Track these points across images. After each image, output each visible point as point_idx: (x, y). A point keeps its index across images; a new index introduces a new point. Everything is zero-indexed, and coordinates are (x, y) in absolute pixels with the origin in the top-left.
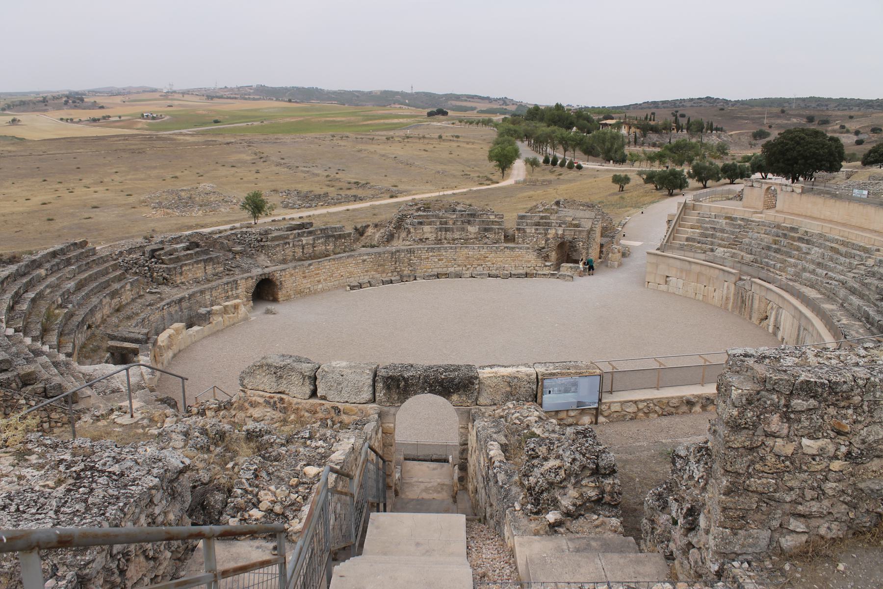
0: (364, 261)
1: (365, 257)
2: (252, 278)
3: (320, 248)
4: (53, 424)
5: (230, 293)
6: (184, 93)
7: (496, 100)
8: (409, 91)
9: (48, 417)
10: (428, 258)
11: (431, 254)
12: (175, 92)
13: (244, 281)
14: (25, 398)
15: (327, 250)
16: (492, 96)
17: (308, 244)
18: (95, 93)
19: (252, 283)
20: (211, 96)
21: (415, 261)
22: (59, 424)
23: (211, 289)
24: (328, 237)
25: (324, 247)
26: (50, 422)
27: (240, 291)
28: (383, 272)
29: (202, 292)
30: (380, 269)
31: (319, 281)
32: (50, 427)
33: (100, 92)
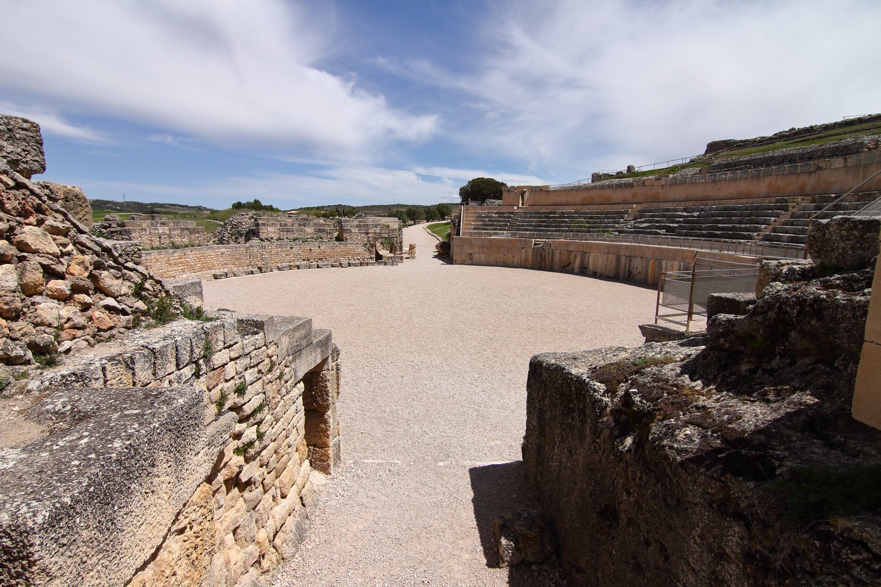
0: (223, 254)
17: (164, 234)
28: (240, 266)
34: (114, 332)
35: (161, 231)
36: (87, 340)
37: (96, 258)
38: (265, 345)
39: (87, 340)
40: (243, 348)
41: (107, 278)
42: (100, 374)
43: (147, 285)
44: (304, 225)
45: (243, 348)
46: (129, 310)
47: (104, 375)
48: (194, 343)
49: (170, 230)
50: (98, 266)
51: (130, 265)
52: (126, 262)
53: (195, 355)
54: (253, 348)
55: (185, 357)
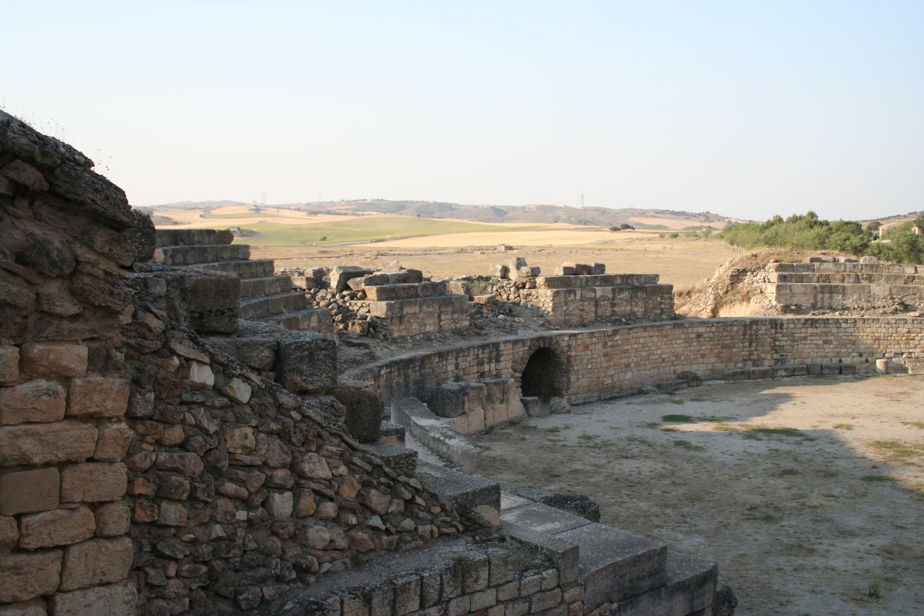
0: (699, 335)
1: (702, 330)
2: (523, 342)
3: (623, 308)
4: (307, 501)
5: (486, 367)
6: (279, 208)
7: (695, 216)
8: (578, 205)
9: (292, 467)
10: (805, 338)
11: (810, 330)
12: (267, 207)
13: (510, 346)
14: (214, 363)
15: (633, 313)
16: (689, 211)
17: (604, 298)
18: (165, 207)
19: (523, 351)
20: (313, 211)
21: (784, 342)
22: (329, 508)
23: (459, 352)
24: (635, 289)
25: (628, 308)
26: (297, 490)
27: (502, 364)
28: (730, 359)
29: (442, 355)
30: (725, 353)
31: (628, 366)
32: (296, 513)
33: (173, 208)
34: (372, 555)
35: (599, 293)
36: (344, 563)
37: (365, 477)
38: (559, 586)
39: (344, 563)
40: (519, 589)
41: (376, 498)
42: (338, 606)
43: (419, 500)
44: (870, 279)
45: (519, 589)
46: (393, 530)
47: (342, 606)
48: (445, 581)
49: (614, 291)
50: (366, 485)
51: (402, 478)
52: (399, 475)
53: (445, 595)
54: (538, 589)
55: (433, 595)
